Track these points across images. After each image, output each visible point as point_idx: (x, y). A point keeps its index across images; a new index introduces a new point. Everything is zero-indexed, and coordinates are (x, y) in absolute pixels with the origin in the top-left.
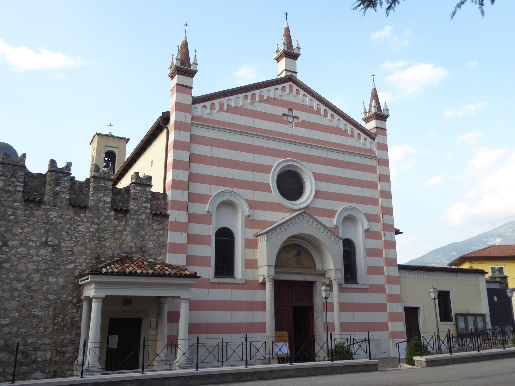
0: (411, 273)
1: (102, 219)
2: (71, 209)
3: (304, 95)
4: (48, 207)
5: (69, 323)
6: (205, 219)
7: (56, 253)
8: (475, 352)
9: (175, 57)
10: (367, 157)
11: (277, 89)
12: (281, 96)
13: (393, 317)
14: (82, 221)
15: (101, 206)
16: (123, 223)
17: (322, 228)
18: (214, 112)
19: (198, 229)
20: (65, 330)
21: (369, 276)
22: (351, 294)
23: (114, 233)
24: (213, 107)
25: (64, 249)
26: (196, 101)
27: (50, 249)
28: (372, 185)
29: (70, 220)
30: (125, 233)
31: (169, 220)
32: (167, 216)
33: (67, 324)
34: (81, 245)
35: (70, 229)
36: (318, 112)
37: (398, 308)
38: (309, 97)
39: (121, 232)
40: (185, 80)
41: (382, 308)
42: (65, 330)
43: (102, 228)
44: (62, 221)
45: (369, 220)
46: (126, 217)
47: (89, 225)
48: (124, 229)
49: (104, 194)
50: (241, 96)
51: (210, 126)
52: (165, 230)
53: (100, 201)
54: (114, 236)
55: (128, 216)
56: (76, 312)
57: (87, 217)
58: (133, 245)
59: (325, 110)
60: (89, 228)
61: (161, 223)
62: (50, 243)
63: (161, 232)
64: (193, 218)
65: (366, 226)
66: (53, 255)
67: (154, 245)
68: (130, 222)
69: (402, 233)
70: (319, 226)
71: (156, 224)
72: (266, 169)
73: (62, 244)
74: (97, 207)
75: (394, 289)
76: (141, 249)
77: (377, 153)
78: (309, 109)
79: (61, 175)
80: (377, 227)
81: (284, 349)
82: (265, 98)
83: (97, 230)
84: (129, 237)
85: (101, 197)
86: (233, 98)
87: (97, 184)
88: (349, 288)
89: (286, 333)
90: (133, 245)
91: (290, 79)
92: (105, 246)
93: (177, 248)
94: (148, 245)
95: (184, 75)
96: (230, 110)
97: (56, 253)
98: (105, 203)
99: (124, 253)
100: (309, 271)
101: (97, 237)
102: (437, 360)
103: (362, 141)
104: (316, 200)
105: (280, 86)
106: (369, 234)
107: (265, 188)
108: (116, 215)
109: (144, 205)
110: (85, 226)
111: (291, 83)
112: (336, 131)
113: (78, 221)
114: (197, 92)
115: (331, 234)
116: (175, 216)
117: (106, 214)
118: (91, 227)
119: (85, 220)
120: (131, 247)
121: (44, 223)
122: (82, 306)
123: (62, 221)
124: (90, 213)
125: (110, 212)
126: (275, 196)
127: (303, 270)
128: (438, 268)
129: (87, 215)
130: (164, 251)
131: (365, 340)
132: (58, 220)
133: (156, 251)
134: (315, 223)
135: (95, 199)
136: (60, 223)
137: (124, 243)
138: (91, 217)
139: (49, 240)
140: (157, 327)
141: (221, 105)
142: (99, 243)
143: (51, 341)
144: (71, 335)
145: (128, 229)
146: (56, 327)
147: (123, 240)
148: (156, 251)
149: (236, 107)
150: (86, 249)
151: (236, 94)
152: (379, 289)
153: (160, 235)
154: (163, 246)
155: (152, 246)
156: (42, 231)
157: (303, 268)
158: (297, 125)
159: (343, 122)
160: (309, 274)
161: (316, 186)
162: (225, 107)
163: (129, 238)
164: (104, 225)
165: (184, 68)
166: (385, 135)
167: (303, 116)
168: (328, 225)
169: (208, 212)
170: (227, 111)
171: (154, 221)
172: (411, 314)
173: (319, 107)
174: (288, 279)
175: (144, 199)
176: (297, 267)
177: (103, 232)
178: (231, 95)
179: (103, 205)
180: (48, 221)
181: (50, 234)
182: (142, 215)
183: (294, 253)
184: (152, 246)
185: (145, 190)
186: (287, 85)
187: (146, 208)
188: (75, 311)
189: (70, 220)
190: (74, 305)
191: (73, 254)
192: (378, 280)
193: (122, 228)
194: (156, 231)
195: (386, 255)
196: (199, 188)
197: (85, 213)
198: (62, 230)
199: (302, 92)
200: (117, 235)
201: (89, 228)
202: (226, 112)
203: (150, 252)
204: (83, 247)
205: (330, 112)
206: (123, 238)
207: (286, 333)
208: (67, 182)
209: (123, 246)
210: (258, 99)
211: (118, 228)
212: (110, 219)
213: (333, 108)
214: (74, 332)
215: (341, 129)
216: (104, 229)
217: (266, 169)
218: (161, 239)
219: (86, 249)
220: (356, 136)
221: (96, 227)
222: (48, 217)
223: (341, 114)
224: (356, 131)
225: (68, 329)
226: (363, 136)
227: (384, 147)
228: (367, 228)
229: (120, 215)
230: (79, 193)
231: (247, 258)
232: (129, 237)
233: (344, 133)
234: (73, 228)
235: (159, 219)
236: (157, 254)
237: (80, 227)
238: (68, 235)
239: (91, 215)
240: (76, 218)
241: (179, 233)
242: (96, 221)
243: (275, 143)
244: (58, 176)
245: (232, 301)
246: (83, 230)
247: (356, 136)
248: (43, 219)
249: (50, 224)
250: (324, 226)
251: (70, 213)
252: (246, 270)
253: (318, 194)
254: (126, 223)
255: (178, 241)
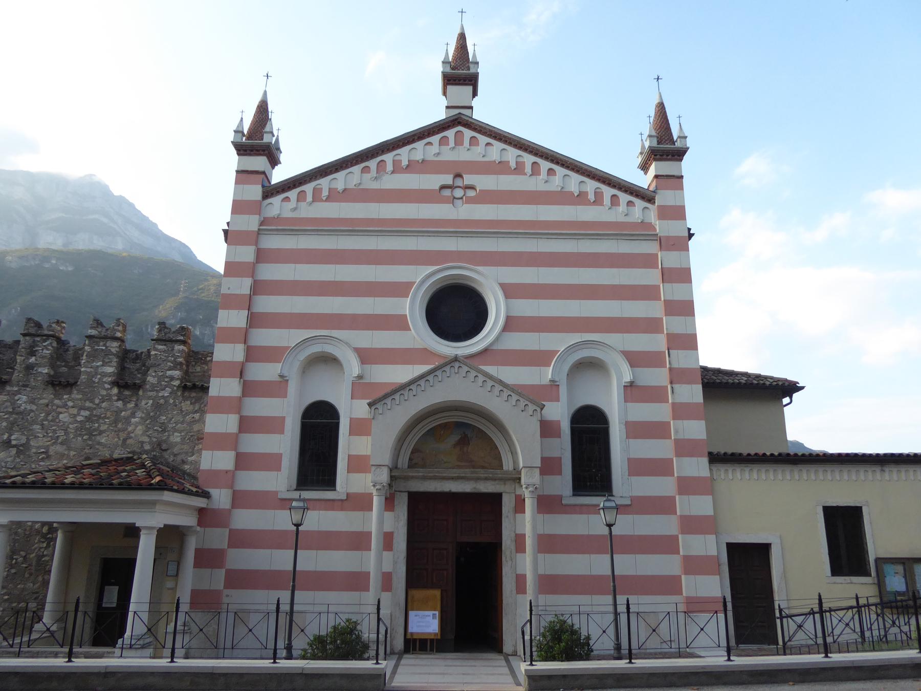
0: (747, 470)
1: (97, 401)
2: (50, 389)
3: (488, 144)
4: (16, 389)
5: (34, 564)
6: (277, 389)
7: (22, 457)
8: (622, 664)
9: (646, 132)
10: (631, 237)
11: (430, 143)
12: (438, 154)
13: (694, 565)
14: (65, 406)
15: (97, 380)
16: (131, 405)
17: (498, 387)
18: (303, 205)
19: (260, 407)
20: (27, 575)
21: (634, 479)
22: (584, 516)
23: (116, 422)
24: (301, 197)
25: (34, 450)
26: (270, 191)
27: (14, 451)
28: (648, 293)
29: (47, 405)
30: (133, 420)
31: (210, 394)
32: (205, 389)
33: (30, 565)
34: (62, 443)
35: (47, 420)
36: (519, 169)
37: (709, 546)
38: (498, 145)
39: (127, 420)
40: (259, 162)
41: (667, 545)
42: (27, 575)
43: (96, 416)
44: (34, 407)
45: (632, 365)
46: (137, 394)
47: (75, 411)
48: (133, 415)
49: (103, 361)
50: (356, 169)
51: (292, 230)
52: (202, 412)
53: (96, 374)
54: (116, 426)
55: (141, 393)
56: (46, 548)
57: (73, 400)
58: (146, 439)
59: (534, 163)
60: (75, 416)
61: (198, 400)
62: (14, 443)
63: (197, 416)
64: (250, 389)
65: (627, 377)
66: (18, 460)
67: (183, 439)
68: (144, 402)
69: (802, 388)
70: (490, 383)
71: (189, 402)
72: (399, 290)
73: (32, 443)
74: (90, 383)
75: (701, 505)
76: (159, 444)
77: (662, 227)
78: (501, 168)
79: (38, 339)
80: (657, 377)
81: (427, 623)
82: (405, 163)
83: (88, 419)
84: (140, 427)
85: (98, 367)
86: (341, 175)
87: (92, 348)
88: (582, 505)
89: (437, 593)
90: (146, 439)
91: (459, 120)
92: (99, 443)
93: (222, 441)
94: (172, 439)
95: (250, 155)
96: (334, 196)
97: (22, 457)
98: (105, 375)
99: (129, 453)
100: (482, 473)
101: (88, 429)
102: (564, 676)
103: (622, 208)
104: (506, 334)
105: (435, 139)
106: (632, 391)
107: (399, 323)
108: (120, 392)
109: (169, 373)
110: (69, 412)
111: (460, 128)
112: (562, 198)
113: (58, 407)
114: (279, 175)
115: (517, 397)
116: (222, 387)
117: (104, 393)
118: (78, 414)
119: (70, 404)
120: (142, 443)
121: (7, 413)
122: (56, 538)
123: (34, 407)
124: (78, 394)
125: (111, 389)
126: (420, 335)
127: (467, 472)
128: (885, 455)
129: (73, 396)
130: (200, 446)
131: (812, 613)
132: (29, 407)
133: (186, 447)
134: (481, 378)
135: (89, 370)
136: (32, 411)
137: (131, 438)
138: (81, 400)
139: (13, 437)
140: (177, 575)
141: (317, 192)
142: (90, 439)
143: (5, 591)
144: (34, 584)
145: (139, 414)
146: (13, 571)
147: (129, 433)
148: (186, 447)
149: (345, 190)
150: (69, 449)
151: (347, 167)
152: (663, 506)
153: (195, 421)
154: (200, 439)
155: (178, 440)
156: (4, 424)
157: (474, 467)
158: (470, 201)
159: (575, 178)
160: (486, 479)
161: (508, 308)
162: (325, 193)
163: (140, 429)
164: (100, 410)
165: (257, 143)
166: (682, 188)
167: (484, 182)
168: (510, 381)
169: (281, 376)
170: (329, 199)
171: (185, 399)
172: (749, 565)
173: (520, 159)
174: (439, 490)
175: (169, 364)
176: (459, 467)
177: (97, 421)
178: (337, 171)
179: (100, 379)
180: (13, 409)
181: (16, 428)
182: (164, 389)
183: (454, 438)
184: (178, 440)
185: (173, 350)
186: (450, 133)
187: (172, 378)
188: (45, 545)
189: (47, 405)
190: (44, 536)
191: (48, 457)
192: (662, 486)
193: (129, 412)
194: (187, 414)
195: (676, 432)
196: (265, 337)
197: (70, 393)
198: (34, 422)
199: (483, 139)
200: (120, 426)
201: (75, 416)
202: (326, 201)
203: (176, 450)
204: (65, 447)
205: (545, 165)
206: (130, 429)
207: (437, 593)
208: (48, 349)
209: (129, 441)
210: (390, 167)
211: (123, 413)
212: (110, 400)
213: (552, 156)
214: (40, 579)
215: (572, 193)
216: (99, 417)
217: (399, 290)
218: (196, 427)
219: (69, 449)
220: (607, 200)
221: (87, 413)
222: (13, 403)
223: (571, 164)
224: (608, 192)
225: (31, 574)
226: (624, 198)
227: (679, 213)
228: (628, 380)
229: (127, 393)
230: (72, 364)
231: (353, 453)
232: (140, 427)
233: (581, 199)
234: (50, 418)
235: (193, 394)
236: (187, 453)
237: (61, 416)
238: (43, 428)
239: (80, 396)
240: (57, 402)
241: (224, 416)
242: (88, 404)
243: (421, 239)
244: (34, 341)
245: (319, 532)
246: (65, 420)
247: (607, 200)
248: (6, 407)
249: (17, 414)
250: (501, 382)
251: (48, 396)
252: (351, 475)
253: (511, 324)
254: (136, 405)
255: (221, 430)
